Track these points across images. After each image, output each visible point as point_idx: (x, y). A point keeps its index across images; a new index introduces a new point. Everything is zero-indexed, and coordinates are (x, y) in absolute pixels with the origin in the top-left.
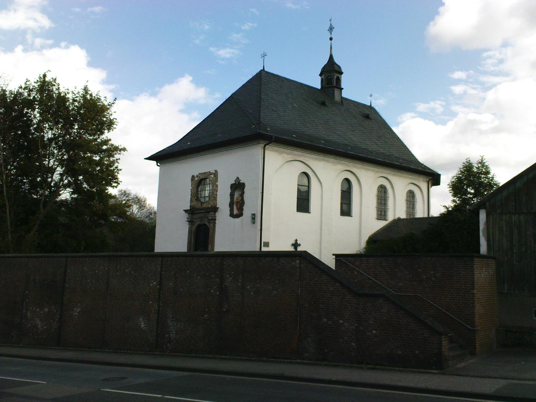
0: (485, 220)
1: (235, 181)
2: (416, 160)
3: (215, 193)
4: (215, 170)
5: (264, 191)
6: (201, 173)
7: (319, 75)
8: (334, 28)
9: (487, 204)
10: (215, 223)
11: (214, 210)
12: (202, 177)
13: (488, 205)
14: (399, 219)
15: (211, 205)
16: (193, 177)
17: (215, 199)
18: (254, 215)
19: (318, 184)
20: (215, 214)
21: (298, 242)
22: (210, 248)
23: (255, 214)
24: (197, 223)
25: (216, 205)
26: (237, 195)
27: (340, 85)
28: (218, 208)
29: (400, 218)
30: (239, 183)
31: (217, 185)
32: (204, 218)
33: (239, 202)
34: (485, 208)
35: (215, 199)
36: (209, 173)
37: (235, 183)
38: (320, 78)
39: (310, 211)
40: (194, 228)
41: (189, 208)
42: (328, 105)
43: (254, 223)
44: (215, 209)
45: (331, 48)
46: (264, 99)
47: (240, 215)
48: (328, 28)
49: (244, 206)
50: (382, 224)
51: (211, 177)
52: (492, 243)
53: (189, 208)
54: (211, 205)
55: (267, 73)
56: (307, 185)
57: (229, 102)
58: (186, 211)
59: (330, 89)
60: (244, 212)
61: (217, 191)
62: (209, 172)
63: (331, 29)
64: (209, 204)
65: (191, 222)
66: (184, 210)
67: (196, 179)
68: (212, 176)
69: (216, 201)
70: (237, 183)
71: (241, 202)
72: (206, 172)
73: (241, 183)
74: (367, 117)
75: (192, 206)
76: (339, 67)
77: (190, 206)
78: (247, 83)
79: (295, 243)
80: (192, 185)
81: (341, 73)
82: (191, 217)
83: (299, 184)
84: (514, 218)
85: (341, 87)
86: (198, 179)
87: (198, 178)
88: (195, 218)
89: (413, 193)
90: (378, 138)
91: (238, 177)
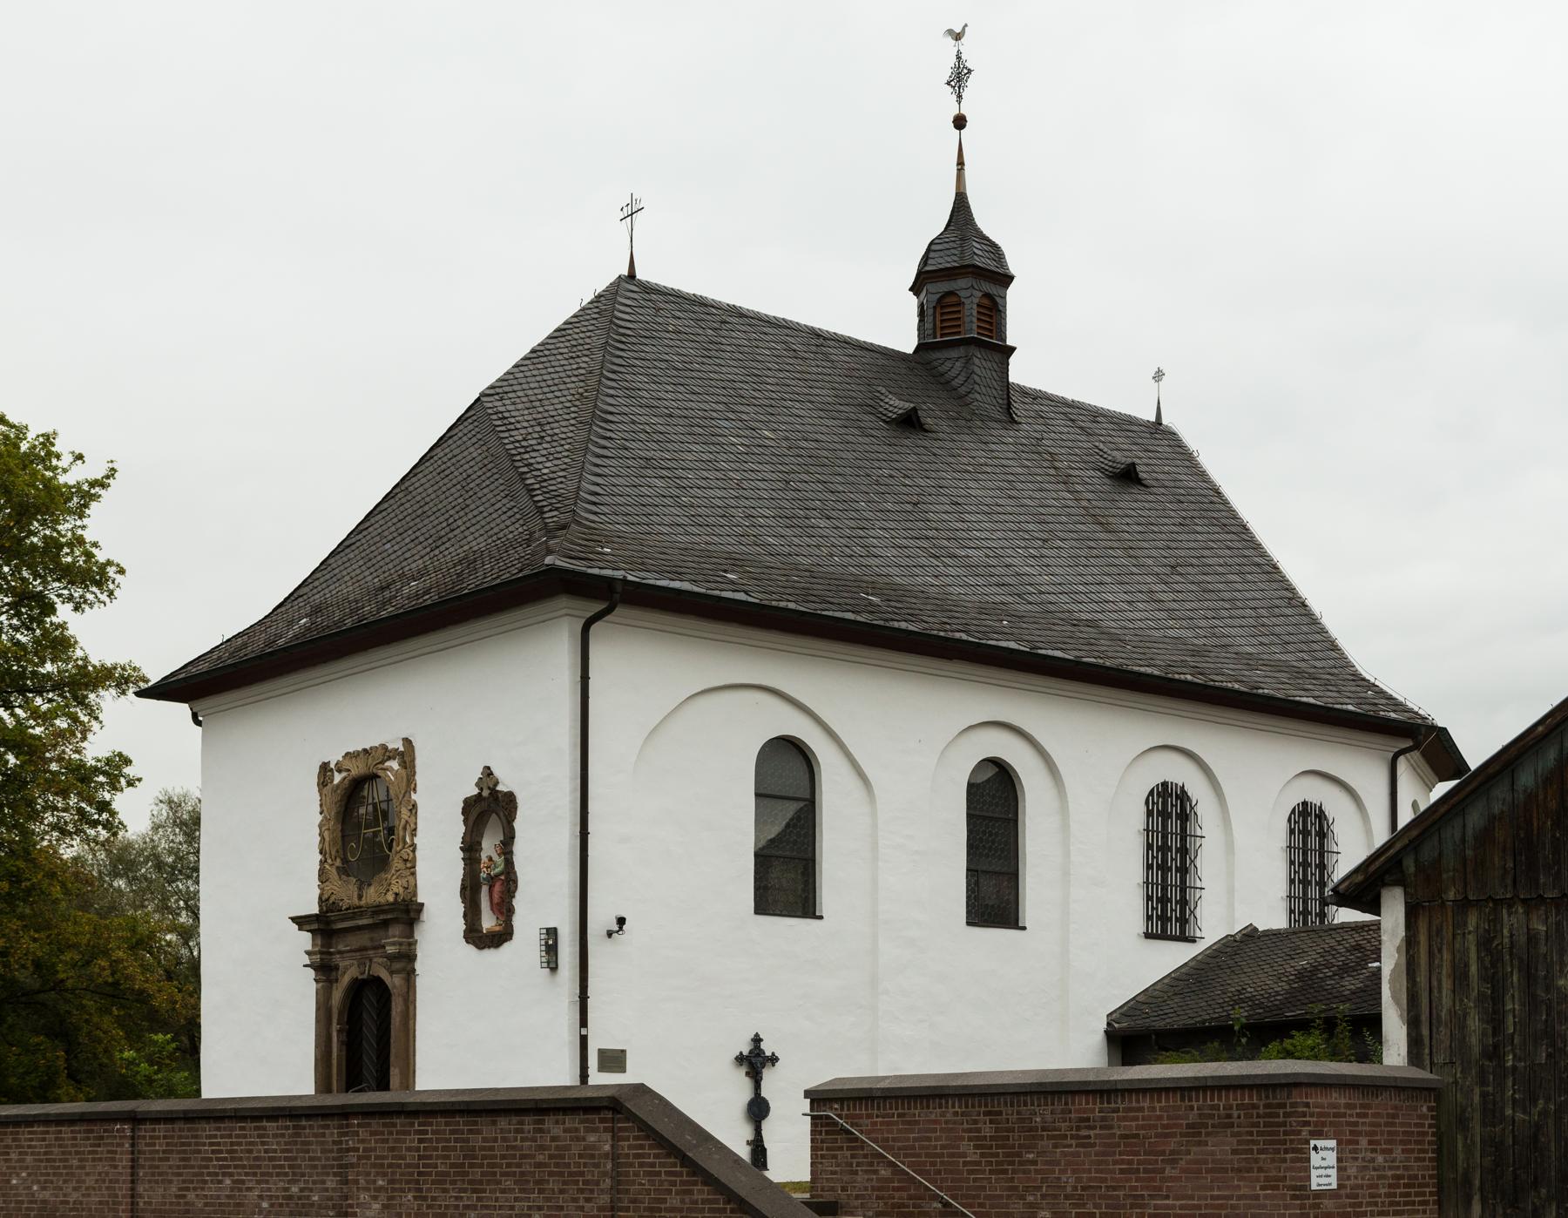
0: (1402, 932)
1: (477, 785)
2: (1343, 663)
3: (408, 840)
4: (403, 739)
5: (590, 829)
6: (351, 750)
7: (911, 289)
8: (970, 71)
9: (1410, 865)
10: (410, 975)
11: (404, 916)
12: (357, 769)
13: (1412, 869)
14: (1250, 934)
15: (397, 894)
16: (325, 768)
17: (409, 865)
18: (552, 933)
19: (853, 783)
20: (411, 935)
21: (763, 1045)
22: (395, 1080)
23: (555, 929)
24: (350, 972)
25: (415, 894)
26: (489, 846)
27: (1002, 335)
28: (422, 905)
29: (1256, 929)
30: (494, 792)
31: (415, 806)
32: (371, 952)
33: (497, 876)
34: (1401, 882)
35: (409, 865)
36: (380, 751)
37: (480, 794)
38: (913, 301)
39: (821, 911)
40: (337, 995)
41: (315, 910)
42: (935, 428)
43: (553, 966)
44: (408, 911)
45: (961, 163)
46: (611, 413)
47: (501, 937)
48: (947, 73)
49: (517, 894)
50: (1172, 957)
51: (390, 769)
52: (1425, 1032)
53: (315, 910)
54: (397, 894)
55: (649, 289)
56: (808, 797)
57: (471, 427)
58: (301, 922)
59: (954, 353)
60: (518, 921)
61: (415, 830)
62: (384, 747)
63: (959, 77)
64: (388, 890)
65: (324, 968)
66: (293, 919)
67: (338, 778)
68: (394, 765)
69: (414, 874)
70: (486, 793)
71: (503, 877)
72: (371, 748)
73: (500, 792)
74: (1127, 476)
75: (327, 900)
76: (995, 251)
77: (320, 898)
78: (550, 341)
79: (751, 1052)
80: (321, 805)
81: (1007, 279)
82: (322, 946)
83: (760, 792)
84: (1512, 922)
85: (1005, 341)
86: (344, 778)
87: (344, 774)
88: (340, 952)
89: (1321, 815)
90: (1168, 570)
91: (489, 768)
